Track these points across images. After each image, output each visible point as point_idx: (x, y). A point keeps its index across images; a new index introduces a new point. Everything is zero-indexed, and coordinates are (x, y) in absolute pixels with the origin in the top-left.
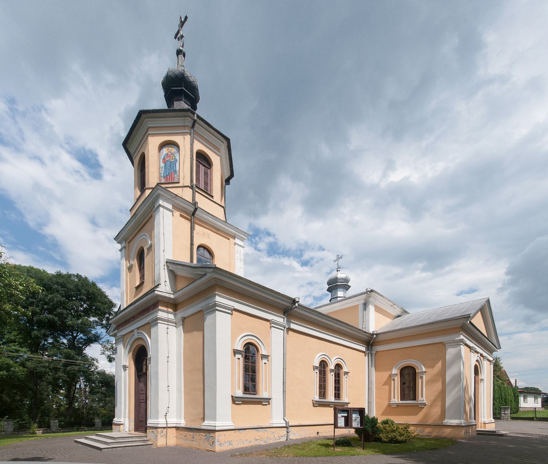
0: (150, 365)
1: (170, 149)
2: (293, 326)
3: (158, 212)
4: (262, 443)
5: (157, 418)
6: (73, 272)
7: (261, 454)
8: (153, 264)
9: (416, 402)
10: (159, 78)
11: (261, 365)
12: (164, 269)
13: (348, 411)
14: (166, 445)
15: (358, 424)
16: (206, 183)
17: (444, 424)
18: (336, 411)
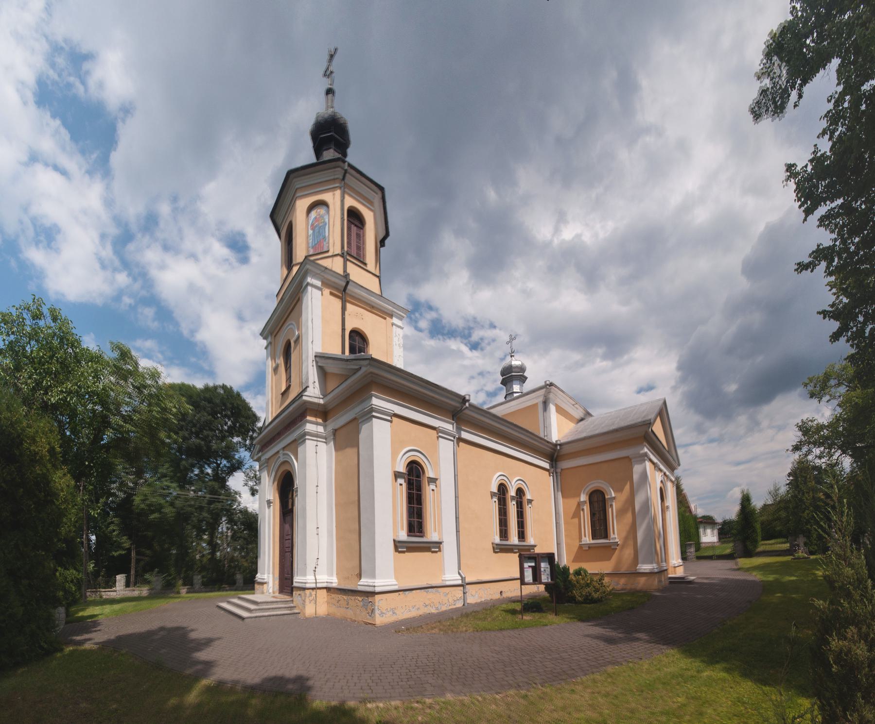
0: (296, 498)
1: (319, 210)
2: (465, 435)
3: (306, 293)
4: (434, 611)
5: (305, 575)
6: (219, 383)
7: (433, 628)
8: (301, 361)
9: (608, 541)
10: (309, 123)
11: (428, 490)
12: (313, 366)
13: (536, 558)
14: (316, 614)
15: (548, 578)
16: (358, 248)
17: (638, 571)
18: (522, 559)
